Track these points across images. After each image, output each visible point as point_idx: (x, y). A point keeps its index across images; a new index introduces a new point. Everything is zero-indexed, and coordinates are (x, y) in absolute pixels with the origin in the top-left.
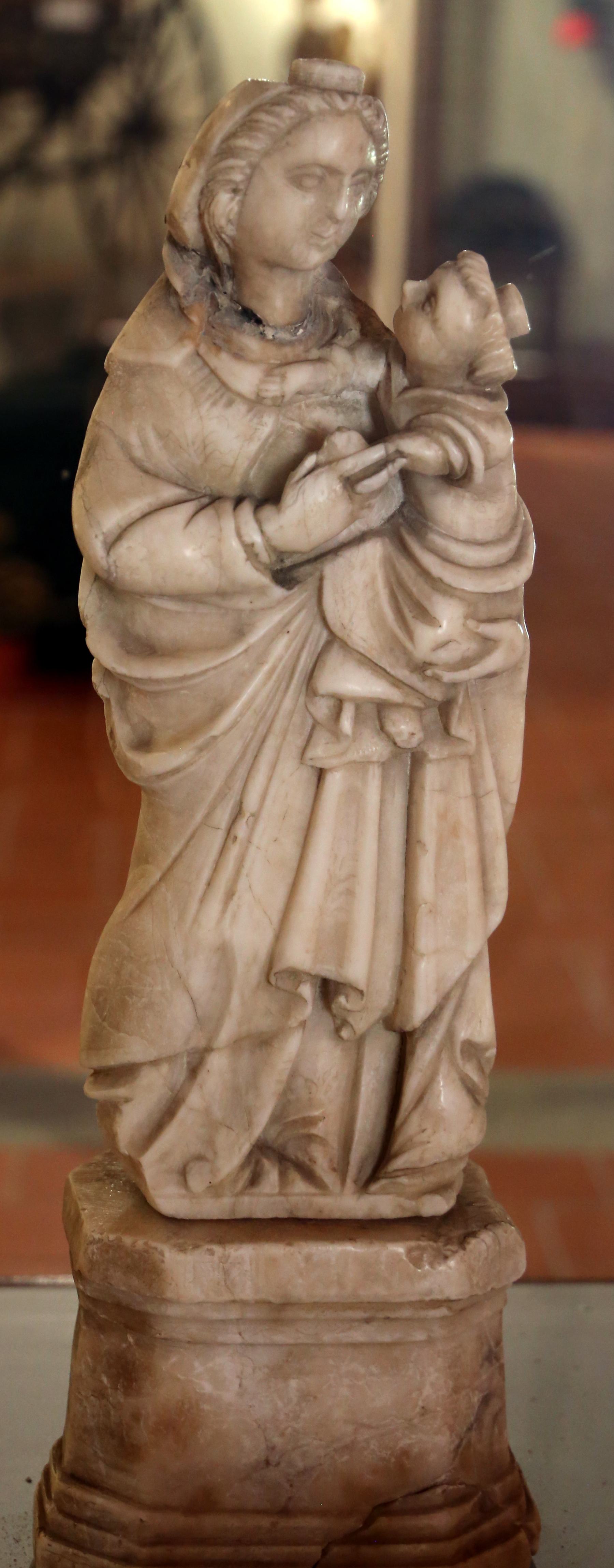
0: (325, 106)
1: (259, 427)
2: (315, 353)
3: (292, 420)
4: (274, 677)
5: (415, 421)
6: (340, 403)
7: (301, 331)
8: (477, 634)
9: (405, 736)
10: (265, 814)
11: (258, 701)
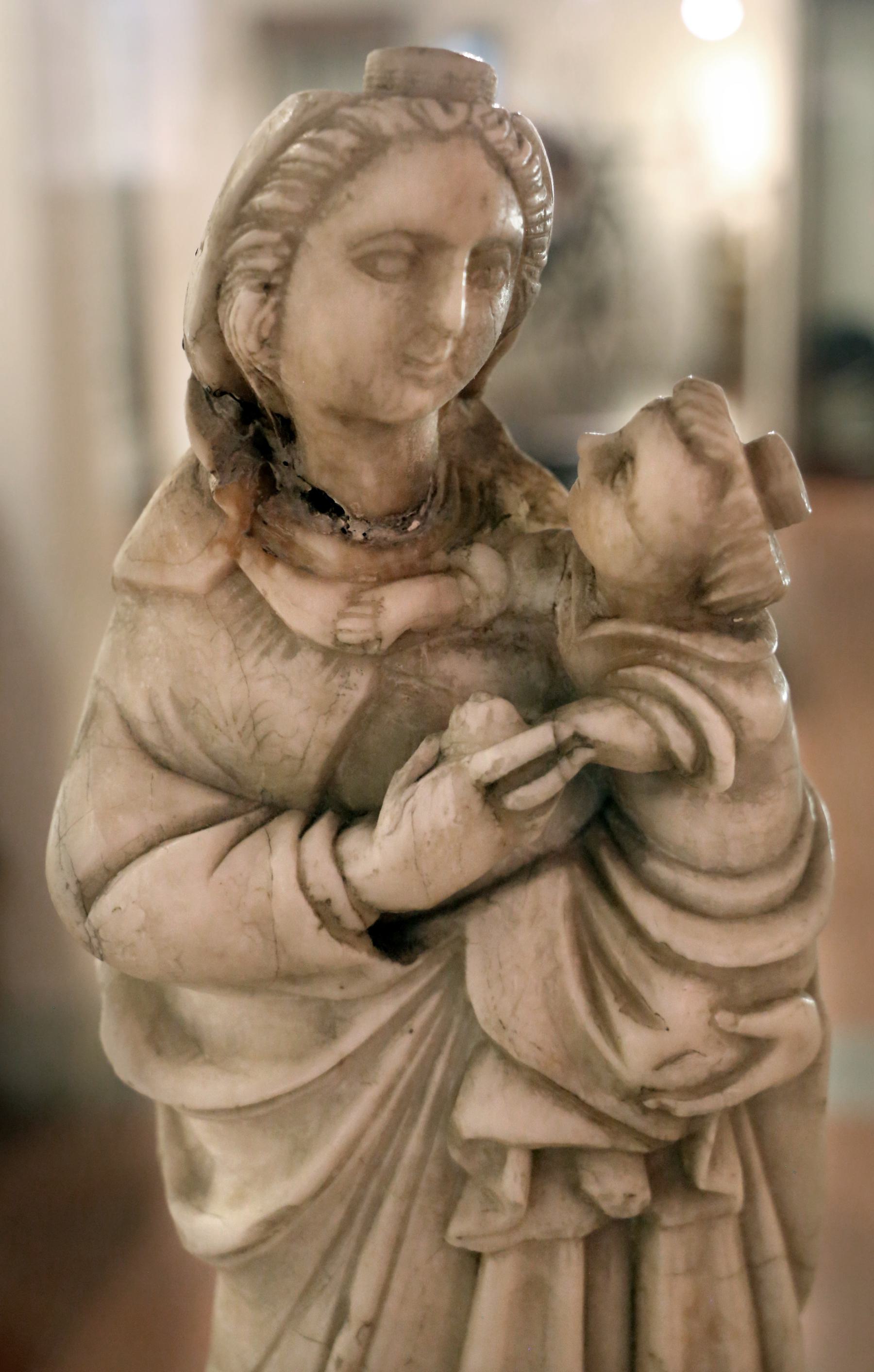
0: (408, 123)
1: (342, 691)
2: (440, 558)
3: (404, 674)
4: (392, 1103)
5: (609, 677)
6: (491, 641)
7: (415, 524)
8: (733, 1035)
9: (618, 1200)
10: (385, 1324)
11: (366, 1144)
